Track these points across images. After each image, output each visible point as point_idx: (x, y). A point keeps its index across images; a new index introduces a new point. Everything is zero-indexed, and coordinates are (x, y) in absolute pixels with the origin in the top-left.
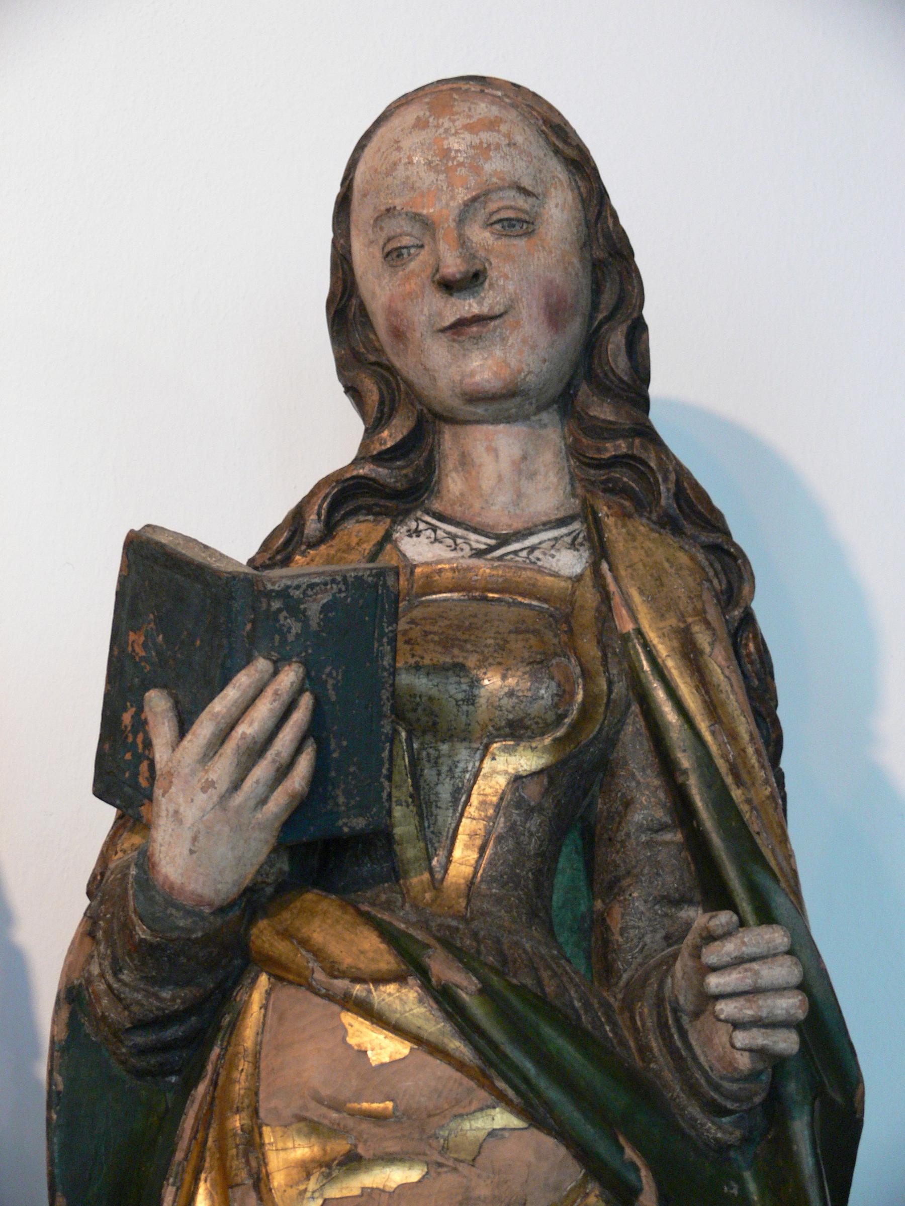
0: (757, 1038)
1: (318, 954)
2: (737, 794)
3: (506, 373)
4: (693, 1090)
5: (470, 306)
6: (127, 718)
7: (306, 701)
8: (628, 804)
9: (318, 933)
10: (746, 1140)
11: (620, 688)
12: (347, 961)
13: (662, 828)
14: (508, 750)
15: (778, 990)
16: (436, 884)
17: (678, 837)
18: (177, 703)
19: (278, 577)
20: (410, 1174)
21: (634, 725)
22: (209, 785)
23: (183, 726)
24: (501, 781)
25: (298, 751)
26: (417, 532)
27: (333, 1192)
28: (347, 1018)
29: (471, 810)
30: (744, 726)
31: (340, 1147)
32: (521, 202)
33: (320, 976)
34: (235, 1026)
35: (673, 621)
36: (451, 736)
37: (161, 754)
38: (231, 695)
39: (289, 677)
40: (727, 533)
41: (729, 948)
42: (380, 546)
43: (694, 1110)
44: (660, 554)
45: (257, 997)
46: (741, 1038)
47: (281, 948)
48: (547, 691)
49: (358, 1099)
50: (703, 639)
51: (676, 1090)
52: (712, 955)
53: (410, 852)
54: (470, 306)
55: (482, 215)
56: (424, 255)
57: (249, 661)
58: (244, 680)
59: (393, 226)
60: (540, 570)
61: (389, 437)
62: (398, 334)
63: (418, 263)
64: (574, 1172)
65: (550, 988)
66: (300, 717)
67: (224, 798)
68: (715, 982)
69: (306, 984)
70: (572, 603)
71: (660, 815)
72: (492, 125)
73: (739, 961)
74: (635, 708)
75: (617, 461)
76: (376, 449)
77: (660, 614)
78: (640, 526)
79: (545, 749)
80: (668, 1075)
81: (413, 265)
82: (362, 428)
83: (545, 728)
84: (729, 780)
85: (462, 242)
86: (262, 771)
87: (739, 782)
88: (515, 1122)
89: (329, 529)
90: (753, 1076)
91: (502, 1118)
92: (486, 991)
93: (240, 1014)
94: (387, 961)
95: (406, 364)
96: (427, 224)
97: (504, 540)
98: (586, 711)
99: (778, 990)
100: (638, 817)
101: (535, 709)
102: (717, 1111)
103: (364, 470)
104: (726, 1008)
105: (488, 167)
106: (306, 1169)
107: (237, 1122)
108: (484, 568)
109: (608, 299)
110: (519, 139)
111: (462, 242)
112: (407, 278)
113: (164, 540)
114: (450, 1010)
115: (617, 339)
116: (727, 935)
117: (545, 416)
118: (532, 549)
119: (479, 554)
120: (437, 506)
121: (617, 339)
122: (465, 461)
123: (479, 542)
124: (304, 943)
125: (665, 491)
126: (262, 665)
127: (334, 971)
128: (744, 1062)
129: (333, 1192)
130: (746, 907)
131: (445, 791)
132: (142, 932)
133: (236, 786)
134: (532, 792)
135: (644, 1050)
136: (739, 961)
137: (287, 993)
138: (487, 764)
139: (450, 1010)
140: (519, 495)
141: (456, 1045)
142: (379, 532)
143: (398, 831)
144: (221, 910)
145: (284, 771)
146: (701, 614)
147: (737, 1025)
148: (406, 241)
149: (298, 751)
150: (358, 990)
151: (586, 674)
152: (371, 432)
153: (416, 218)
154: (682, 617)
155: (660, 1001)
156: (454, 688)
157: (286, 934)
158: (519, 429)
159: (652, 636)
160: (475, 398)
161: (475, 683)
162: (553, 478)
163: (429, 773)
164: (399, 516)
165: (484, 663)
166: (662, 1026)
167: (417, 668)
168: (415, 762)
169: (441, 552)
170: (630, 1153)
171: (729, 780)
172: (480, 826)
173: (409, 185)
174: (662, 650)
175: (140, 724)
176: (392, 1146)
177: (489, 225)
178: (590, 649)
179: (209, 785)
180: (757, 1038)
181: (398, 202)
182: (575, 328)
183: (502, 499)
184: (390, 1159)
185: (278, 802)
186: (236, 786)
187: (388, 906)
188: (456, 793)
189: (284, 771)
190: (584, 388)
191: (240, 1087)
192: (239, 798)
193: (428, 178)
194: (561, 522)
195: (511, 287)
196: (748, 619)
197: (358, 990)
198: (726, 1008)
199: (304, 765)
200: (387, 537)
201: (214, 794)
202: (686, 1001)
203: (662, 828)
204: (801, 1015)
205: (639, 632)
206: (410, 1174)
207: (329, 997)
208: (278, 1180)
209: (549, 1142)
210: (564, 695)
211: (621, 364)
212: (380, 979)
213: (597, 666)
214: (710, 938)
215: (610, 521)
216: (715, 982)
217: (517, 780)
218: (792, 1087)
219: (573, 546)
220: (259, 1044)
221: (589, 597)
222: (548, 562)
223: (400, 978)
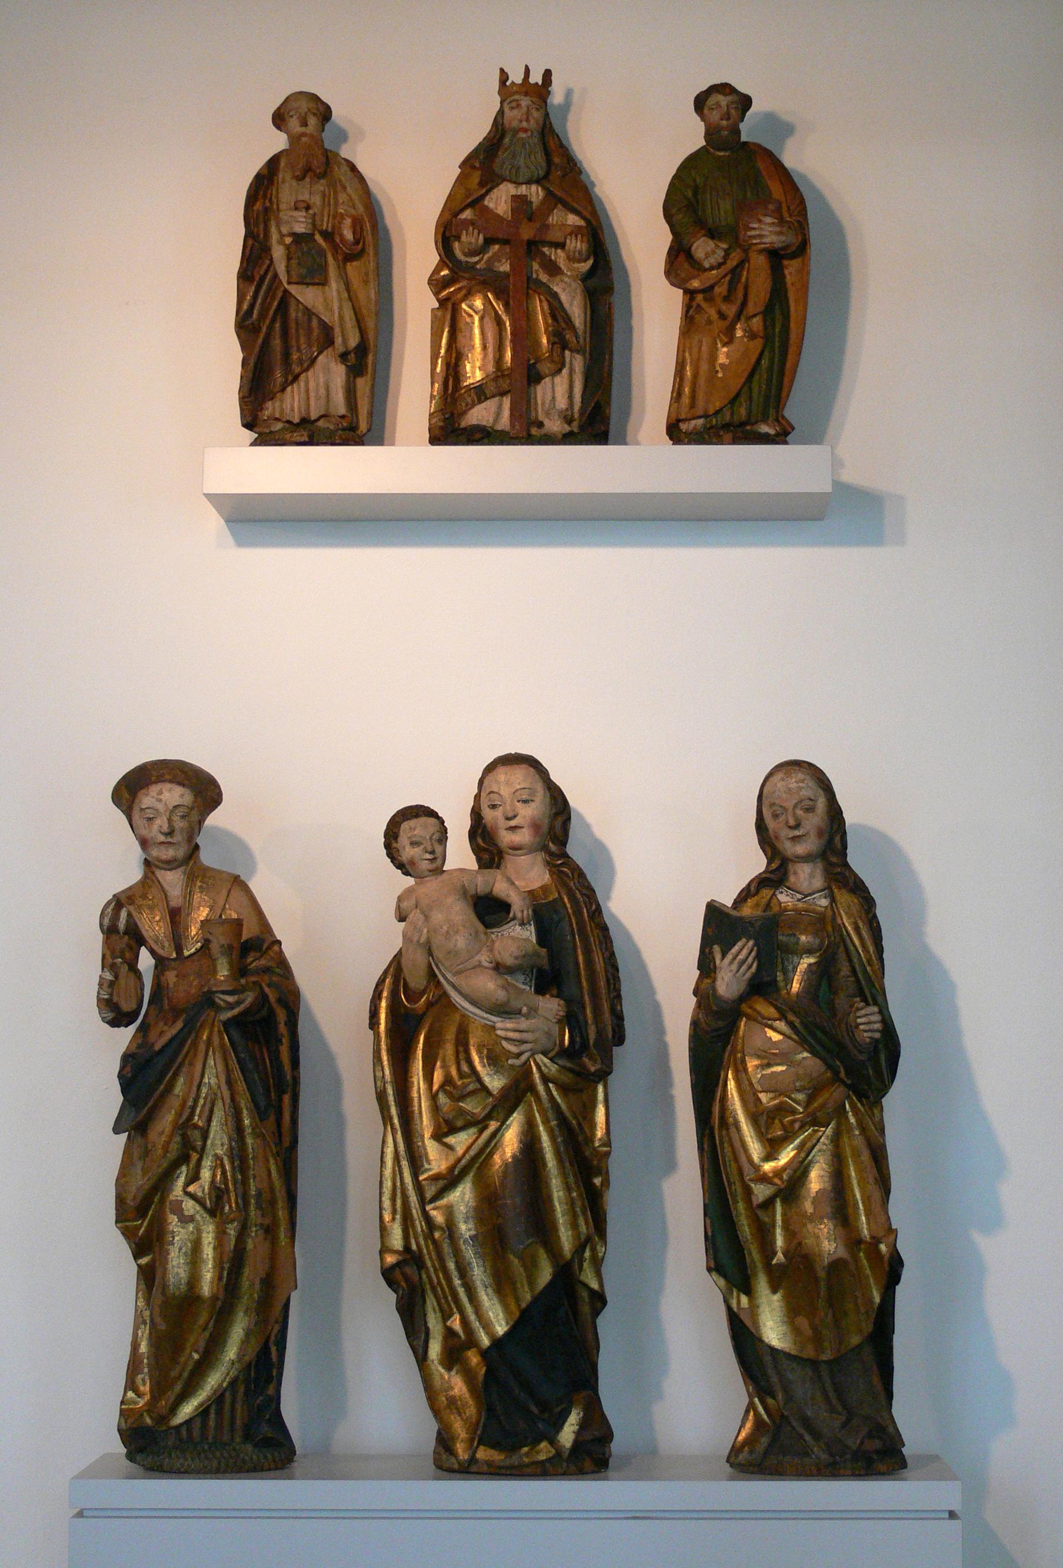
0: (869, 1034)
1: (759, 1013)
2: (868, 968)
3: (807, 851)
4: (855, 1047)
5: (797, 833)
6: (707, 951)
7: (755, 948)
8: (840, 970)
9: (758, 1007)
10: (869, 1059)
11: (837, 940)
12: (766, 1015)
13: (848, 977)
14: (808, 957)
15: (875, 1023)
16: (788, 993)
17: (853, 979)
18: (721, 949)
19: (747, 911)
20: (784, 1068)
21: (841, 949)
22: (731, 971)
23: (724, 956)
24: (805, 966)
25: (753, 962)
26: (782, 893)
27: (764, 1072)
28: (766, 1029)
29: (798, 973)
30: (871, 949)
31: (766, 1061)
32: (811, 803)
33: (759, 1018)
34: (737, 1031)
35: (853, 920)
36: (792, 953)
37: (718, 962)
38: (736, 948)
39: (751, 943)
40: (869, 893)
41: (863, 1012)
42: (771, 898)
43: (855, 1052)
44: (849, 899)
45: (743, 1023)
46: (866, 1034)
47: (749, 1011)
48: (817, 941)
49: (770, 1049)
50: (861, 925)
51: (851, 1047)
52: (859, 1014)
53: (782, 984)
54: (797, 833)
55: (799, 807)
56: (784, 816)
57: (740, 939)
58: (740, 944)
59: (776, 808)
60: (816, 905)
61: (774, 866)
62: (777, 838)
63: (782, 818)
64: (823, 1068)
65: (818, 1020)
66: (753, 954)
67: (735, 975)
68: (859, 1020)
69: (755, 1020)
70: (825, 916)
71: (848, 973)
72: (803, 781)
73: (866, 1015)
74: (842, 944)
75: (838, 873)
76: (771, 869)
77: (849, 918)
78: (844, 891)
79: (818, 957)
80: (848, 1043)
81: (781, 819)
82: (766, 861)
83: (816, 951)
84: (866, 964)
85: (794, 814)
86: (744, 967)
87: (869, 965)
88: (809, 1055)
89: (757, 893)
90: (870, 1043)
91: (806, 1054)
92: (802, 1023)
93: (739, 1027)
94: (776, 1015)
95: (778, 845)
96: (785, 809)
97: (806, 896)
98: (828, 946)
99: (875, 1023)
100: (842, 974)
101: (814, 946)
102: (861, 1052)
103: (768, 875)
104: (862, 1027)
105: (801, 793)
106: (757, 1067)
107: (739, 1055)
108: (800, 905)
109: (835, 827)
110: (810, 784)
111: (794, 814)
112: (778, 823)
113: (717, 905)
114: (437, 1266)
115: (837, 839)
116: (862, 1009)
117: (818, 860)
118: (814, 899)
119: (799, 900)
120: (787, 884)
121: (837, 839)
122: (795, 873)
123: (799, 896)
124: (755, 1010)
125: (851, 881)
126: (744, 940)
127: (764, 1018)
128: (868, 1040)
129: (764, 1072)
130: (870, 1000)
131: (790, 968)
132: (715, 1008)
133: (738, 971)
134: (814, 968)
135: (843, 1037)
136: (866, 1015)
137: (751, 1023)
138: (802, 961)
139: (437, 1266)
140: (810, 882)
141: (794, 1036)
142: (772, 892)
143: (778, 979)
144: (733, 1001)
145: (750, 967)
146: (860, 917)
147: (865, 1031)
148: (778, 812)
149: (753, 962)
150: (769, 1022)
151: (828, 936)
152: (769, 864)
153: (781, 806)
154: (855, 918)
155: (846, 1024)
156: (793, 940)
157: (751, 1007)
158: (811, 865)
159: (847, 924)
160: (798, 857)
161: (799, 939)
162: (820, 878)
163: (786, 963)
164: (777, 888)
165: (801, 934)
166: (847, 1030)
167: (783, 935)
168: (782, 959)
169: (788, 899)
170: (838, 1063)
171: (866, 964)
172: (800, 978)
173: (779, 797)
174: (849, 928)
175: (711, 953)
176: (778, 1061)
177: (801, 809)
178: (830, 929)
179: (731, 971)
180: (869, 1034)
181: (777, 802)
182: (826, 837)
183: (805, 884)
184: (778, 1064)
185: (748, 975)
186: (738, 971)
187: (776, 1000)
188: (793, 968)
189: (750, 967)
190: (829, 853)
191: (739, 1047)
192: (738, 974)
193: (784, 796)
194: (822, 890)
195: (808, 827)
196: (875, 916)
197: (769, 1022)
198: (862, 1027)
199: (755, 965)
200: (774, 894)
201: (732, 973)
202: (853, 1024)
203: (848, 977)
204: (881, 1028)
205: (843, 924)
206: (784, 1068)
207: (762, 1024)
208: (750, 1070)
209: (818, 1061)
210: (822, 942)
211: (839, 846)
212: (775, 1020)
213: (831, 934)
214: (858, 1009)
215: (836, 890)
216: (859, 1020)
217: (810, 965)
218: (880, 1046)
219: (825, 898)
220: (744, 1037)
221: (829, 913)
222: (818, 903)
223: (780, 1020)
